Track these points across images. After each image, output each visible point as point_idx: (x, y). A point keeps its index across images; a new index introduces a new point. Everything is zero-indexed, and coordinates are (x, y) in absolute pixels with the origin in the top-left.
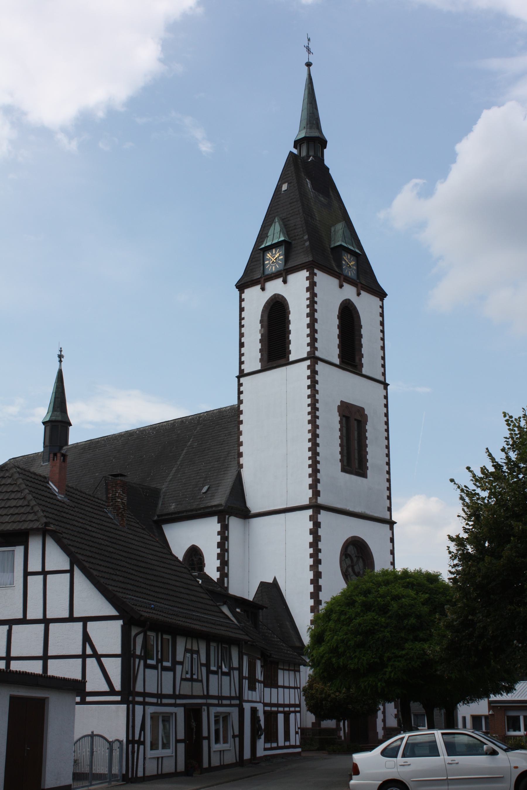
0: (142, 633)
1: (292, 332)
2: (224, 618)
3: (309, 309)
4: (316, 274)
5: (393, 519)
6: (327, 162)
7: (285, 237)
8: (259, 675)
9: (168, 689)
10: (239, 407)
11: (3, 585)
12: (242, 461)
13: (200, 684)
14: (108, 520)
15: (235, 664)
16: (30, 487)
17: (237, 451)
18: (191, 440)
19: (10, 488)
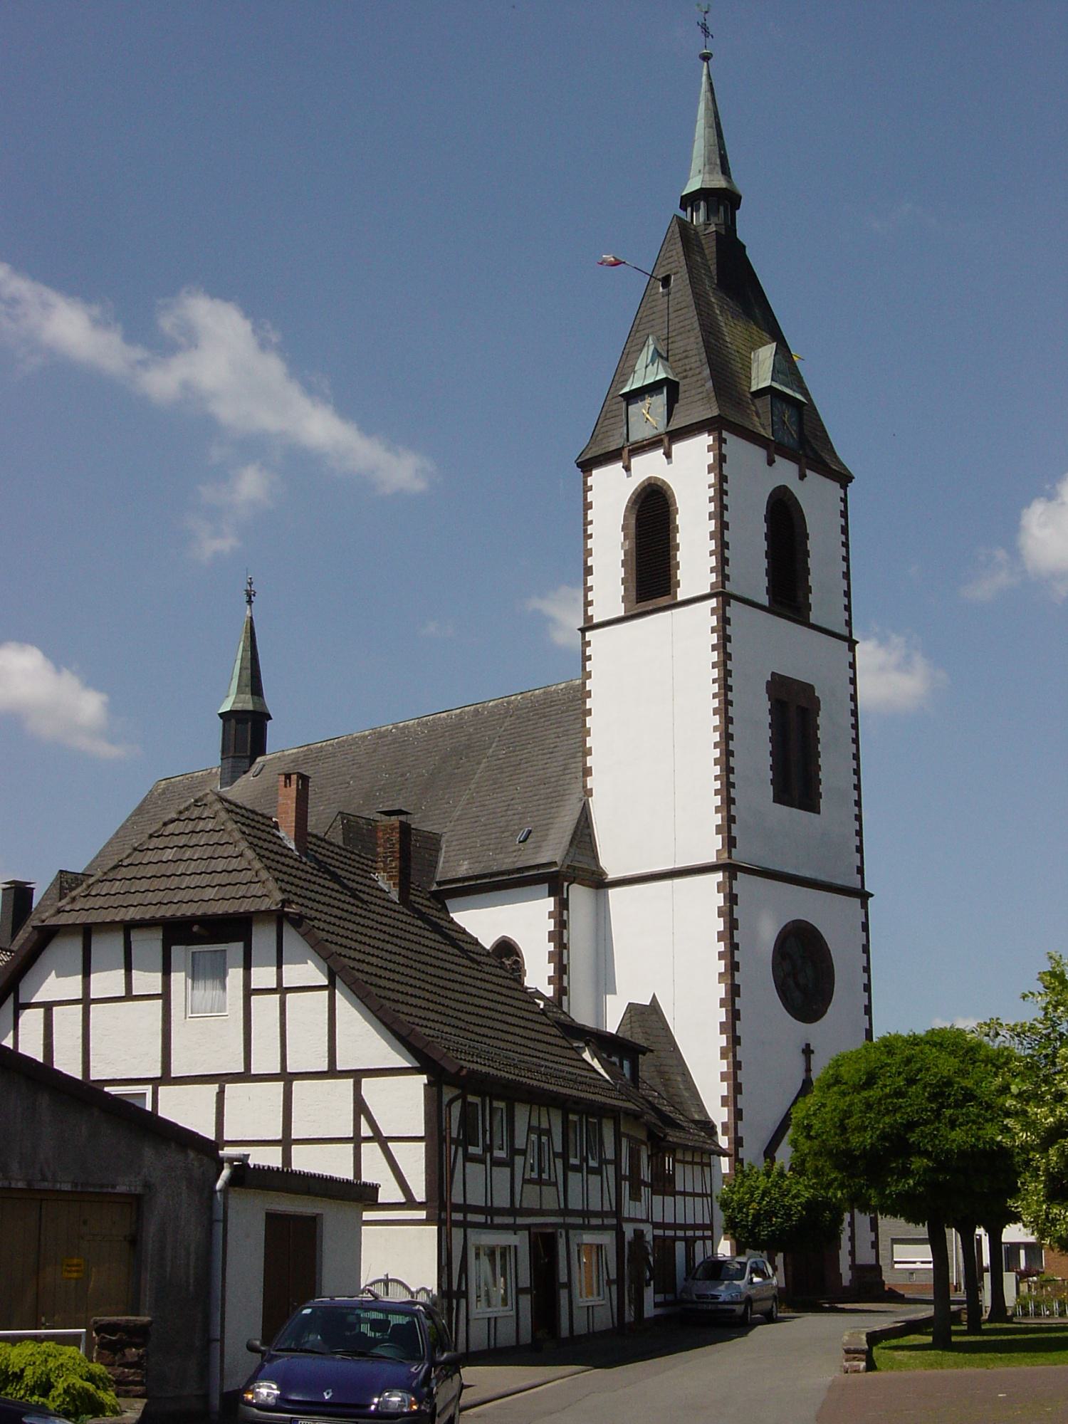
0: (459, 1099)
1: (681, 547)
2: (588, 1070)
3: (713, 504)
4: (725, 441)
5: (866, 889)
6: (741, 235)
7: (666, 372)
8: (646, 1174)
9: (502, 1200)
10: (584, 684)
11: (198, 1013)
12: (590, 782)
13: (553, 1189)
14: (379, 894)
15: (610, 1154)
16: (249, 835)
17: (581, 764)
18: (494, 745)
19: (215, 838)
